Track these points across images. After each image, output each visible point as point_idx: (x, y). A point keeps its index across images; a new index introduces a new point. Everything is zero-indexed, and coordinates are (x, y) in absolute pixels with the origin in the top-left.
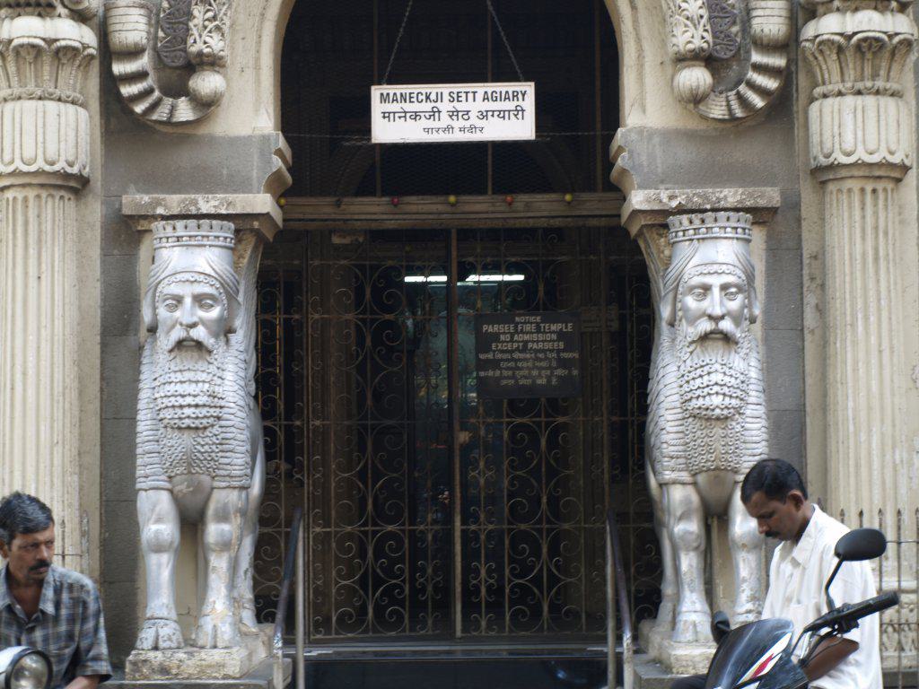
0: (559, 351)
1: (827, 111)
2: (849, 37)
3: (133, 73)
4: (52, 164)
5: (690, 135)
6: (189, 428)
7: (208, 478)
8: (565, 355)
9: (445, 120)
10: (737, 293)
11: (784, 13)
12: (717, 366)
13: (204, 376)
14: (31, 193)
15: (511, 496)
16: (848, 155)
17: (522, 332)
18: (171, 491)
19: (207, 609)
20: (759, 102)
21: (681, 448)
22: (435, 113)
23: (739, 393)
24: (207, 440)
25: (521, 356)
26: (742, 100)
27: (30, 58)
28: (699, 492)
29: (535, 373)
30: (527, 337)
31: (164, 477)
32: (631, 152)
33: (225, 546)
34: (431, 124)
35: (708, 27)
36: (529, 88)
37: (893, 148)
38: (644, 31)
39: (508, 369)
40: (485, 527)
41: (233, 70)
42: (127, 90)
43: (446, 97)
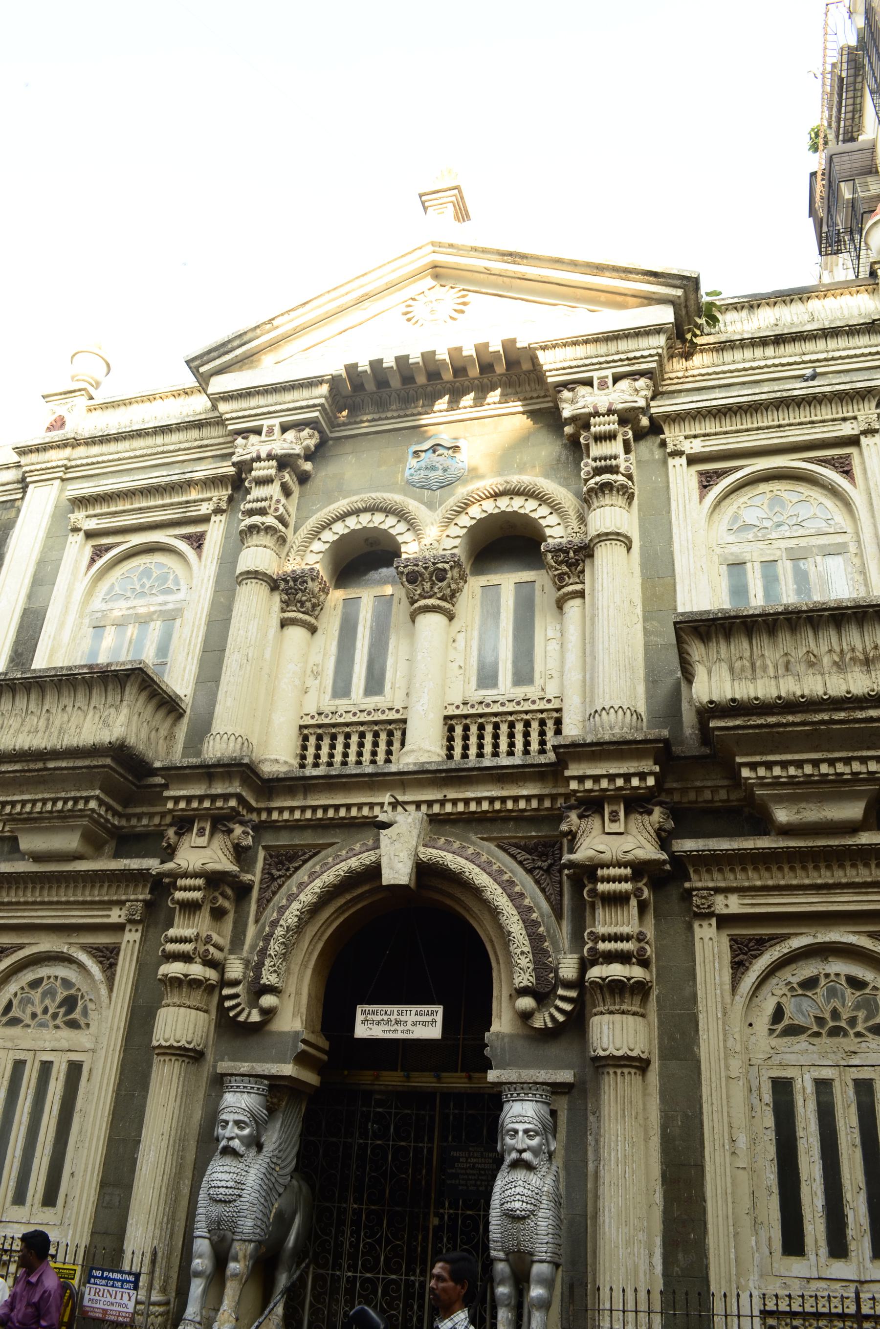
2: (604, 979)
3: (25, 972)
4: (178, 1042)
6: (220, 1201)
7: (230, 1233)
11: (576, 966)
12: (521, 1183)
16: (604, 1050)
17: (473, 1157)
18: (209, 1239)
21: (499, 1235)
23: (533, 1201)
24: (231, 1209)
25: (471, 1172)
26: (552, 1017)
27: (176, 985)
29: (478, 1183)
30: (475, 1160)
31: (206, 1230)
32: (491, 1047)
34: (386, 1028)
35: (533, 974)
37: (632, 1047)
39: (463, 1179)
42: (228, 1004)
43: (396, 1013)
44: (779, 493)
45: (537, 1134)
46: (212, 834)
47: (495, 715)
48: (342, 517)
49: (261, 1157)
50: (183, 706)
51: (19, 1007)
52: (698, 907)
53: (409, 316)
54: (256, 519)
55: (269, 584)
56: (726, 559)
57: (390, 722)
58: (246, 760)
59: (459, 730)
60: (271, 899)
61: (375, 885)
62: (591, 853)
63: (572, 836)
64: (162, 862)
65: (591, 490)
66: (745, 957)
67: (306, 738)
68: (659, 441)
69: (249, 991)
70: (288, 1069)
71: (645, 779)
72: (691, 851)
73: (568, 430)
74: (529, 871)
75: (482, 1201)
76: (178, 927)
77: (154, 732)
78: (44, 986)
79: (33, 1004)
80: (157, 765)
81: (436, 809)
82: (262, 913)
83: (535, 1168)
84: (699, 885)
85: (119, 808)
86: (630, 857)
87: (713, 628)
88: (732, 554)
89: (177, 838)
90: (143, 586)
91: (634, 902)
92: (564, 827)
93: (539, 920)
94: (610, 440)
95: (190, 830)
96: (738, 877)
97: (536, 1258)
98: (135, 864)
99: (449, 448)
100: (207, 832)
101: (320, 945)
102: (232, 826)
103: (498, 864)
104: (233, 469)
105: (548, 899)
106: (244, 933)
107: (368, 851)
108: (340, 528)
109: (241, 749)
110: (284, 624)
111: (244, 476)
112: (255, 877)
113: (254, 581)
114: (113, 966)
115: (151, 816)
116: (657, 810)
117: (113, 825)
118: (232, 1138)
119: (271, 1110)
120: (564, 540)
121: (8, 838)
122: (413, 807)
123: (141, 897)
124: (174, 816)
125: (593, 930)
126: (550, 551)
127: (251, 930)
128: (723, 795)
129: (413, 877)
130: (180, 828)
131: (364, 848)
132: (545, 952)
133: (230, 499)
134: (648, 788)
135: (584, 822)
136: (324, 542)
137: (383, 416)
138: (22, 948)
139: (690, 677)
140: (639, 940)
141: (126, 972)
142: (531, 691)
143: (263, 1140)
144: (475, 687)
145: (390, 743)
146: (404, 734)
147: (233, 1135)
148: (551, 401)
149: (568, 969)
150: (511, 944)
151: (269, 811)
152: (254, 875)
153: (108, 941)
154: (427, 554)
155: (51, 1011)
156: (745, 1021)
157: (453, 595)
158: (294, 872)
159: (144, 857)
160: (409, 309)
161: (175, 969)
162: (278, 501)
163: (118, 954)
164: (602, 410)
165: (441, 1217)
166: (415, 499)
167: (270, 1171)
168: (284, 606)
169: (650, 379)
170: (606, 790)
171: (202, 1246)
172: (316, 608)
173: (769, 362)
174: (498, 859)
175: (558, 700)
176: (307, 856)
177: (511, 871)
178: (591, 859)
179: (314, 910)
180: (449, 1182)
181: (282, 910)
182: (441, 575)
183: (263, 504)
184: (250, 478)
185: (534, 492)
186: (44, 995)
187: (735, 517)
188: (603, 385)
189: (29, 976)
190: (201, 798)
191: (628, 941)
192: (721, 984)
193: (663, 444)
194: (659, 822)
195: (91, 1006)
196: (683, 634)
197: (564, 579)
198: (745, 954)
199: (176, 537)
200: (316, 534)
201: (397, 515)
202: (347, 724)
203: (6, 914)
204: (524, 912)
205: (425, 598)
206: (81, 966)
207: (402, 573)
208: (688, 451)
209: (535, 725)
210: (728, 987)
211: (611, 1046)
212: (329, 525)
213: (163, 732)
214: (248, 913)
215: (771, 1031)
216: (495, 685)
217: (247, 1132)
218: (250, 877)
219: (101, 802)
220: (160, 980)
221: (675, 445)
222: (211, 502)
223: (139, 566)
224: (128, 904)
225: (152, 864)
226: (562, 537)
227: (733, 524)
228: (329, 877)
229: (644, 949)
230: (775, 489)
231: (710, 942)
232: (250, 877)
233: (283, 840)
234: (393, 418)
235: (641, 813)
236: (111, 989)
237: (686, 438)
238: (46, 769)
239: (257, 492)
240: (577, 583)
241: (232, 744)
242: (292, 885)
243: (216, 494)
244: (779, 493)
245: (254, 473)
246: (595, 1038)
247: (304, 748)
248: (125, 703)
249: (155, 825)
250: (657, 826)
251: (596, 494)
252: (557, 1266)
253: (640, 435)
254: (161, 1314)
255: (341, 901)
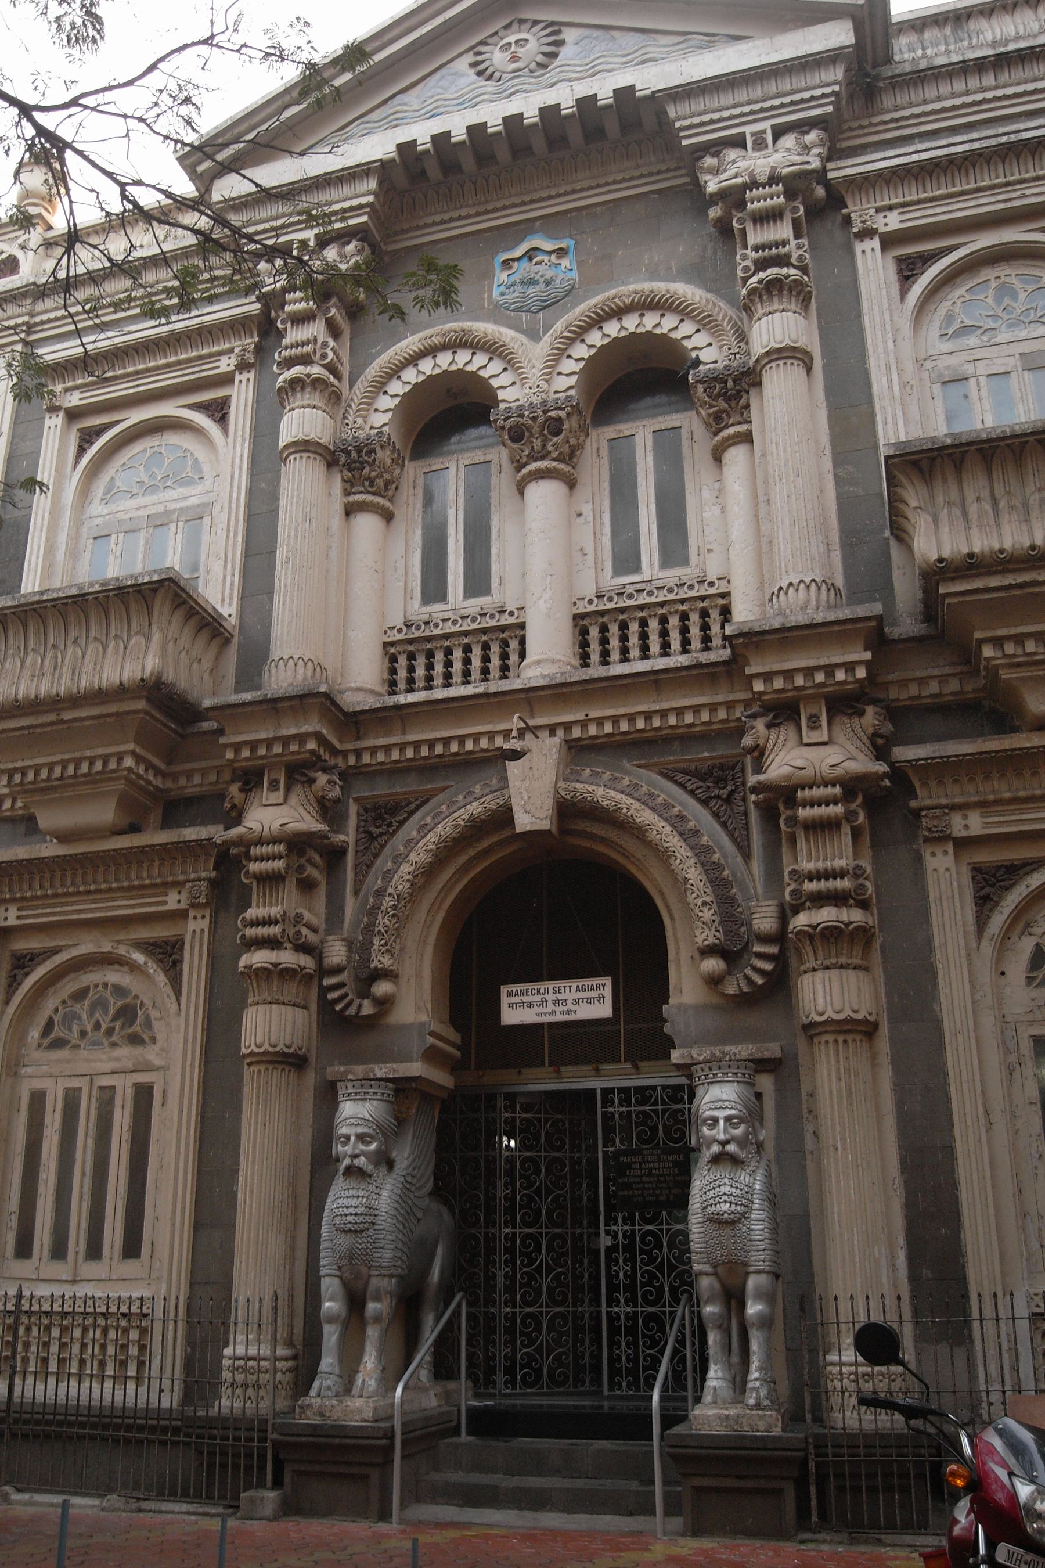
0: (674, 1175)
1: (805, 982)
2: (815, 927)
5: (716, 1008)
6: (350, 1231)
8: (678, 1178)
9: (550, 1007)
10: (739, 1123)
13: (361, 1193)
14: (262, 1068)
15: (643, 1285)
16: (821, 1014)
18: (341, 1278)
19: (361, 1368)
20: (759, 981)
22: (543, 1002)
26: (747, 978)
28: (720, 1281)
29: (658, 1192)
33: (377, 1319)
34: (541, 1010)
36: (608, 982)
37: (856, 1008)
38: (679, 935)
40: (623, 1309)
41: (403, 980)
42: (332, 996)
43: (551, 990)
44: (1008, 279)
45: (742, 1121)
46: (288, 790)
47: (641, 607)
48: (413, 360)
49: (394, 1176)
50: (230, 629)
51: (63, 1024)
52: (929, 830)
53: (481, 67)
54: (297, 371)
55: (325, 458)
56: (941, 375)
57: (503, 629)
58: (323, 689)
59: (594, 633)
60: (372, 863)
61: (506, 834)
62: (786, 770)
63: (759, 753)
64: (226, 829)
65: (752, 292)
66: (993, 890)
67: (393, 659)
68: (839, 218)
69: (357, 979)
70: (415, 1068)
71: (853, 670)
72: (917, 760)
73: (715, 212)
74: (704, 802)
75: (664, 1213)
76: (258, 906)
77: (195, 665)
78: (92, 996)
79: (80, 1018)
80: (207, 703)
81: (576, 733)
82: (362, 882)
83: (743, 1163)
84: (928, 802)
85: (162, 766)
86: (838, 771)
87: (939, 459)
88: (948, 367)
89: (243, 795)
90: (152, 476)
91: (846, 829)
92: (747, 741)
93: (722, 861)
94: (775, 222)
95: (259, 784)
96: (981, 789)
97: (752, 1269)
98: (191, 833)
99: (550, 253)
100: (282, 785)
101: (441, 915)
102: (312, 774)
103: (663, 796)
104: (258, 306)
105: (731, 835)
106: (341, 909)
107: (492, 792)
108: (410, 375)
109: (313, 676)
110: (349, 511)
111: (273, 314)
112: (348, 836)
113: (305, 455)
114: (177, 964)
115: (204, 772)
116: (870, 710)
117: (157, 788)
118: (356, 1156)
119: (401, 1121)
120: (720, 365)
121: (22, 818)
122: (547, 733)
123: (204, 875)
124: (234, 770)
125: (796, 867)
126: (700, 382)
127: (350, 905)
128: (954, 685)
129: (555, 822)
130: (246, 783)
131: (487, 791)
132: (732, 900)
133: (259, 349)
134: (857, 681)
135: (773, 733)
136: (392, 396)
137: (455, 215)
138: (57, 953)
139: (904, 535)
140: (857, 876)
141: (196, 969)
142: (687, 573)
143: (394, 1154)
144: (610, 574)
145: (504, 656)
146: (523, 642)
147: (357, 1151)
148: (687, 175)
149: (765, 920)
150: (689, 893)
151: (358, 753)
152: (347, 835)
153: (167, 934)
154: (535, 400)
155: (104, 1027)
156: (996, 969)
157: (572, 455)
158: (398, 828)
159: (203, 823)
160: (480, 58)
161: (260, 958)
162: (325, 344)
163: (182, 949)
164: (762, 178)
165: (615, 1236)
166: (510, 327)
167: (406, 1191)
168: (348, 486)
169: (825, 129)
170: (803, 688)
171: (330, 1285)
172: (389, 488)
173: (989, 95)
174: (662, 791)
175: (724, 582)
176: (413, 806)
177: (680, 804)
178: (788, 777)
179: (428, 873)
180: (620, 1193)
181: (388, 876)
182: (555, 427)
183: (307, 349)
184: (283, 316)
185: (673, 303)
186: (93, 1007)
187: (950, 318)
188: (760, 144)
189: (69, 986)
190: (269, 743)
191: (842, 878)
192: (964, 924)
193: (847, 221)
194: (874, 725)
195: (154, 1014)
196: (897, 473)
197: (722, 419)
198: (992, 886)
199: (190, 407)
200: (380, 386)
201: (487, 350)
202: (447, 636)
203: (30, 912)
204: (702, 853)
205: (536, 460)
206: (134, 968)
207: (503, 428)
208: (882, 229)
209: (695, 618)
210: (972, 928)
211: (829, 1008)
212: (396, 372)
213: (206, 664)
214: (345, 882)
215: (1030, 980)
216: (637, 569)
217: (373, 1146)
218: (342, 837)
219: (139, 759)
220: (242, 973)
221: (864, 222)
222: (233, 356)
223: (145, 451)
224: (188, 885)
225: (216, 833)
226: (716, 362)
227: (947, 328)
228: (444, 829)
229: (863, 886)
230: (1002, 274)
231: (947, 874)
232: (342, 837)
233: (381, 790)
234: (468, 217)
235: (850, 715)
236: (178, 993)
237: (878, 210)
238: (62, 721)
239: (294, 335)
240: (740, 423)
241: (301, 671)
242: (397, 842)
243: (238, 343)
244: (1008, 279)
245: (287, 308)
246: (806, 1001)
247: (393, 671)
248: (154, 627)
249: (211, 784)
250: (871, 730)
251: (760, 297)
252: (777, 1276)
253: (816, 213)
254: (289, 1370)
255: (463, 859)
